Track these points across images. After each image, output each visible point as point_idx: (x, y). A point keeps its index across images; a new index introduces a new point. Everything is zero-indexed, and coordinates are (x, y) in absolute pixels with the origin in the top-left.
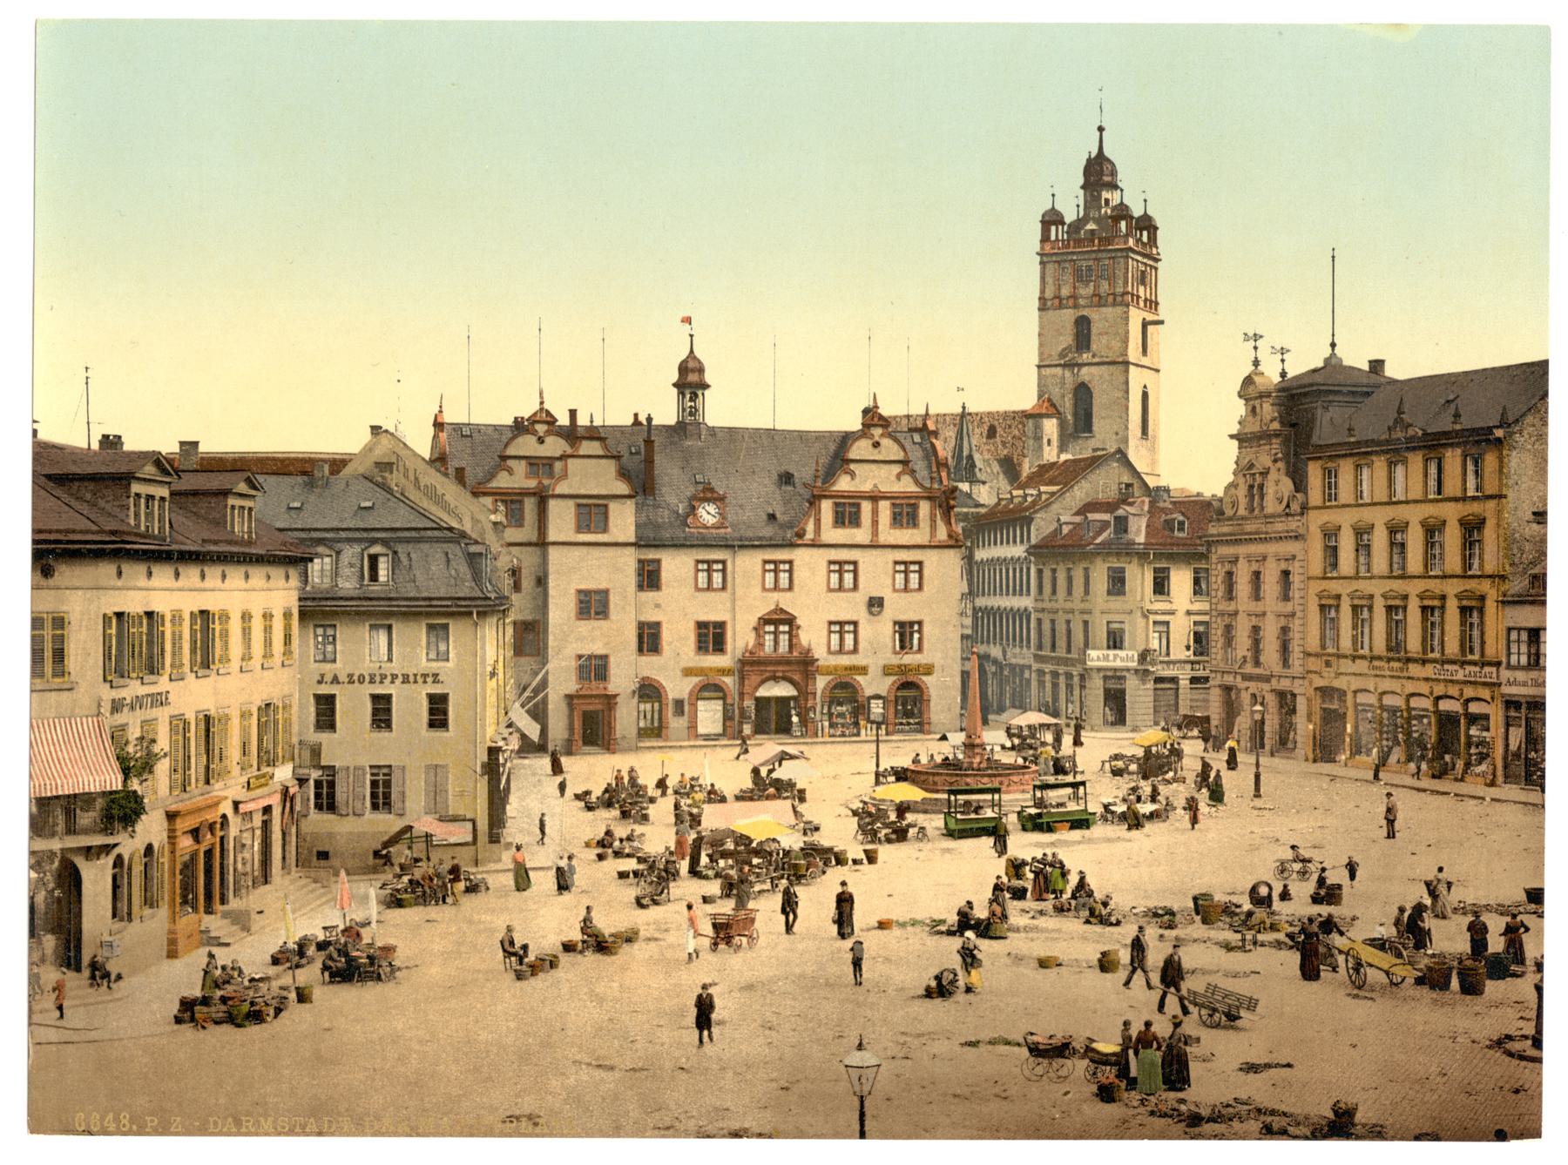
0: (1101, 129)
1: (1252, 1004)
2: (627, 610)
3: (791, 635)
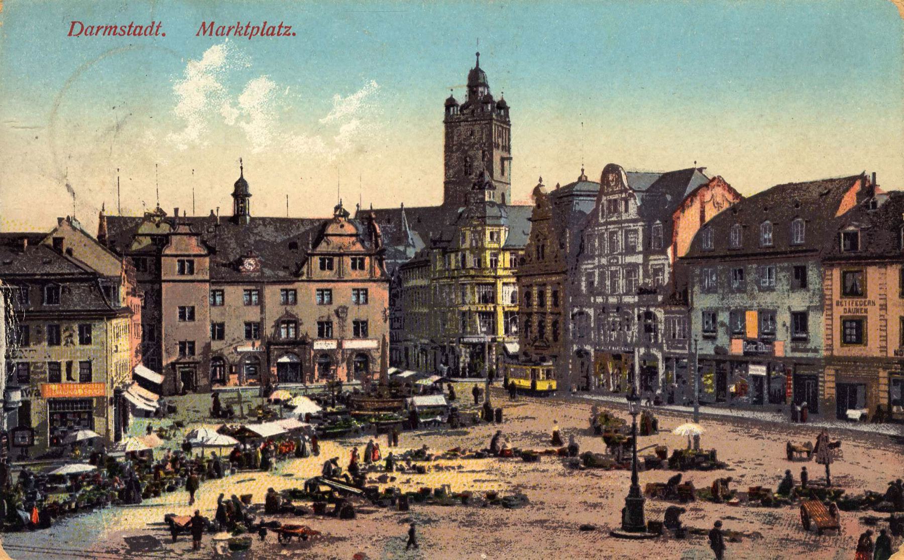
0: (478, 54)
1: (337, 458)
2: (207, 316)
3: (296, 329)
